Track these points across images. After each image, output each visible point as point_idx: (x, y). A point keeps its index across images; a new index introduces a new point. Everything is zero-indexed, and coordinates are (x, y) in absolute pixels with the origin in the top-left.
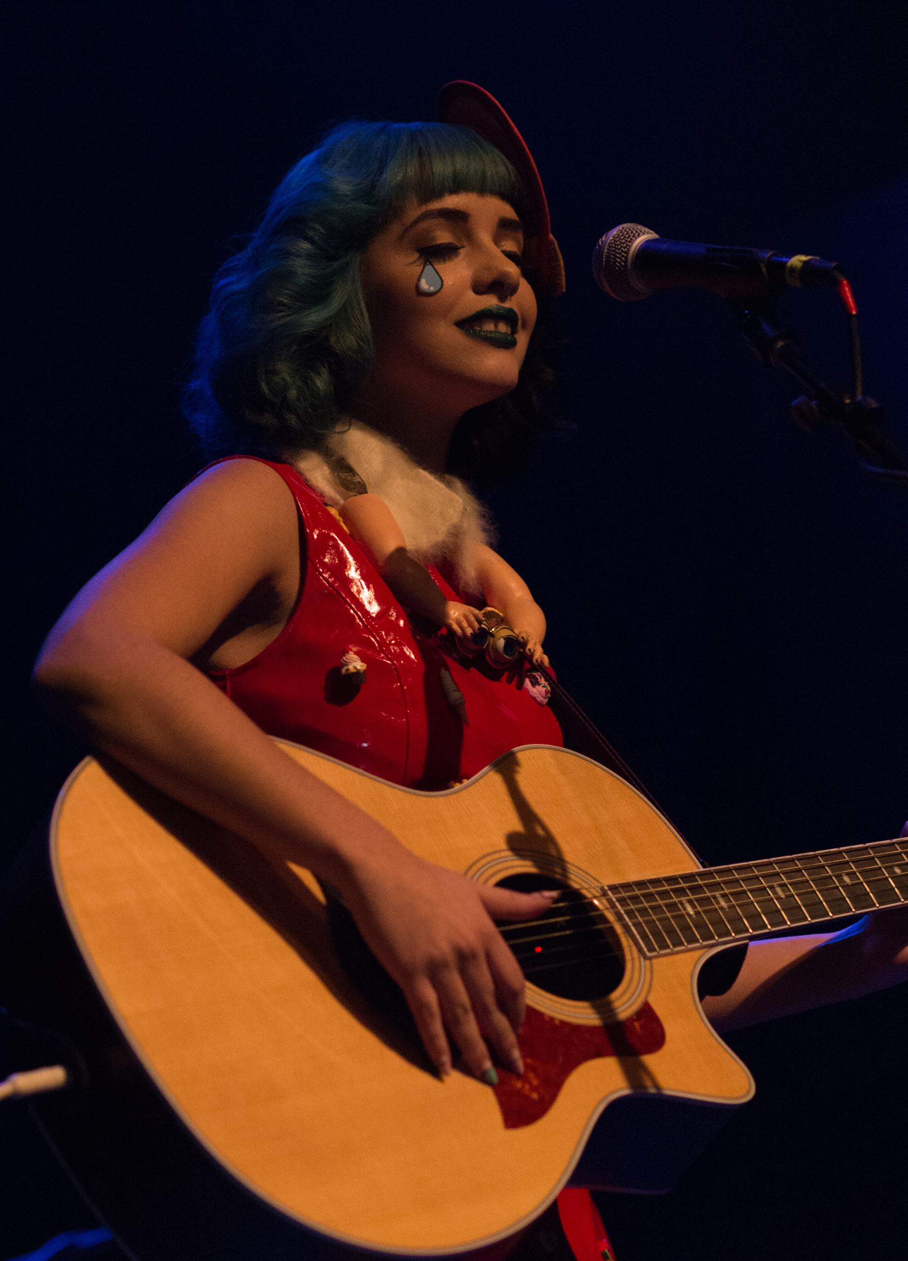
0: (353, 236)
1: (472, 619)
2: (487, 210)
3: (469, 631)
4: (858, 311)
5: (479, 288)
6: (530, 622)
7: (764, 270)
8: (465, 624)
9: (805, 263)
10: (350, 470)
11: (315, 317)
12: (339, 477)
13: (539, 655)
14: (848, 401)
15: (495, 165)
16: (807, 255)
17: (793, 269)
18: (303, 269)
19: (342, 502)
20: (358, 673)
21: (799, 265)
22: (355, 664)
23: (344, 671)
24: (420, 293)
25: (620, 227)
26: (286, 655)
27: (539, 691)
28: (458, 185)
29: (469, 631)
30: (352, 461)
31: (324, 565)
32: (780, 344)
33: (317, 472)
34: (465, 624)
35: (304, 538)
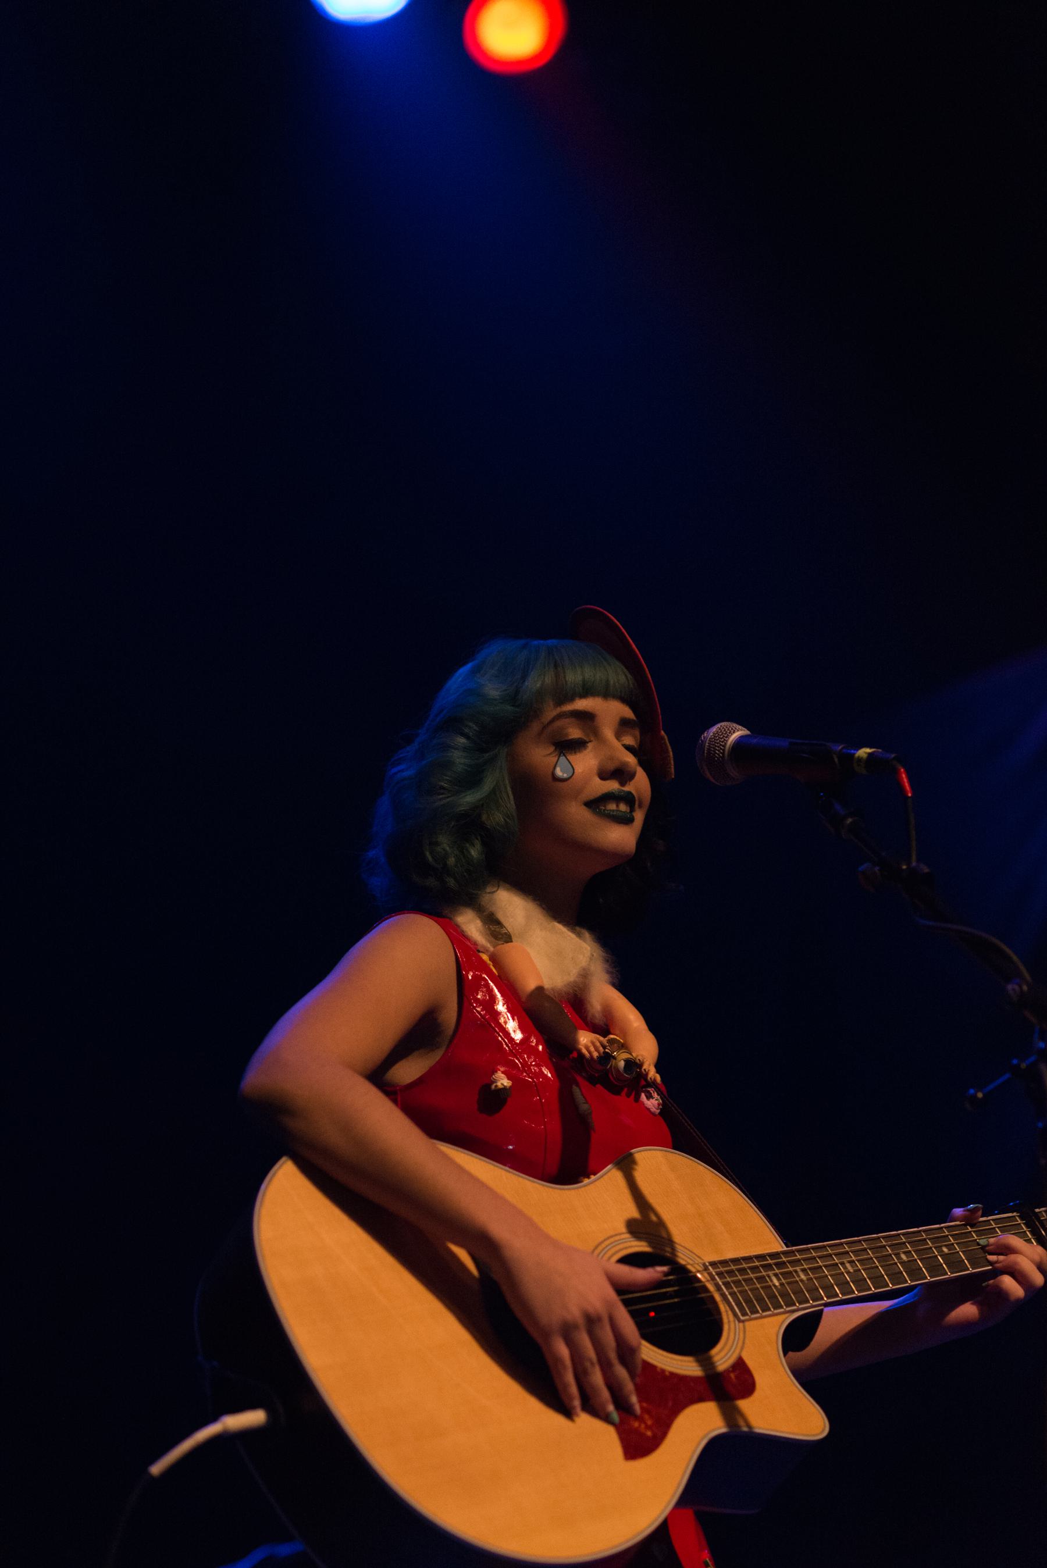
0: (501, 733)
1: (598, 1044)
2: (610, 711)
3: (595, 1054)
4: (913, 793)
5: (603, 775)
6: (645, 1048)
7: (836, 760)
8: (592, 1049)
9: (870, 754)
10: (498, 923)
11: (470, 798)
12: (490, 929)
13: (653, 1074)
14: (904, 867)
15: (617, 675)
16: (871, 748)
17: (860, 759)
18: (459, 760)
19: (492, 949)
20: (505, 1088)
21: (865, 756)
22: (503, 1081)
23: (493, 1087)
24: (556, 779)
25: (719, 725)
26: (445, 1072)
27: (652, 1103)
28: (587, 691)
29: (595, 1054)
30: (500, 916)
31: (477, 1001)
32: (849, 820)
33: (471, 925)
34: (592, 1049)
35: (461, 979)
